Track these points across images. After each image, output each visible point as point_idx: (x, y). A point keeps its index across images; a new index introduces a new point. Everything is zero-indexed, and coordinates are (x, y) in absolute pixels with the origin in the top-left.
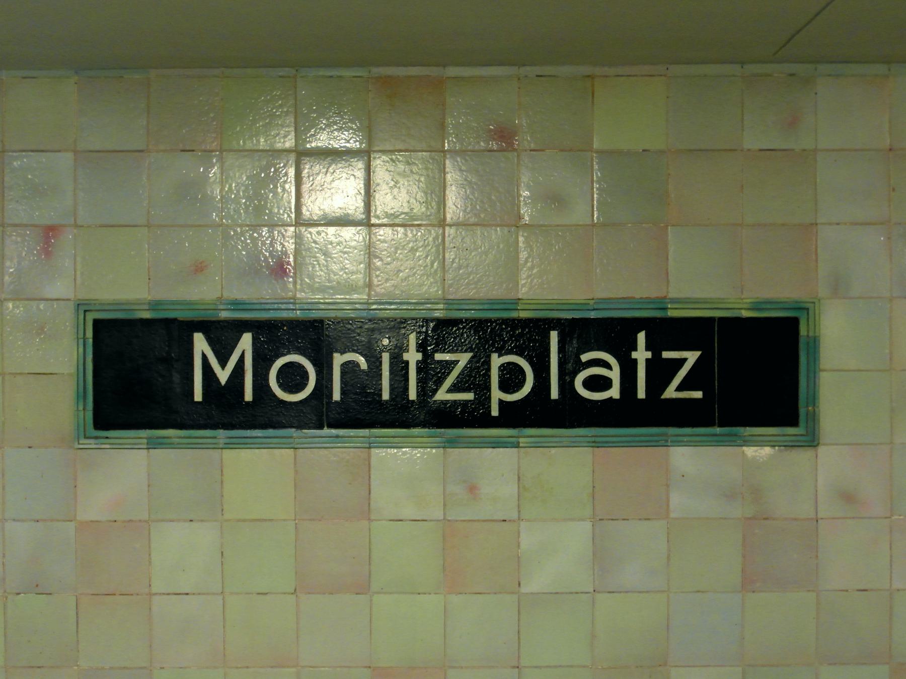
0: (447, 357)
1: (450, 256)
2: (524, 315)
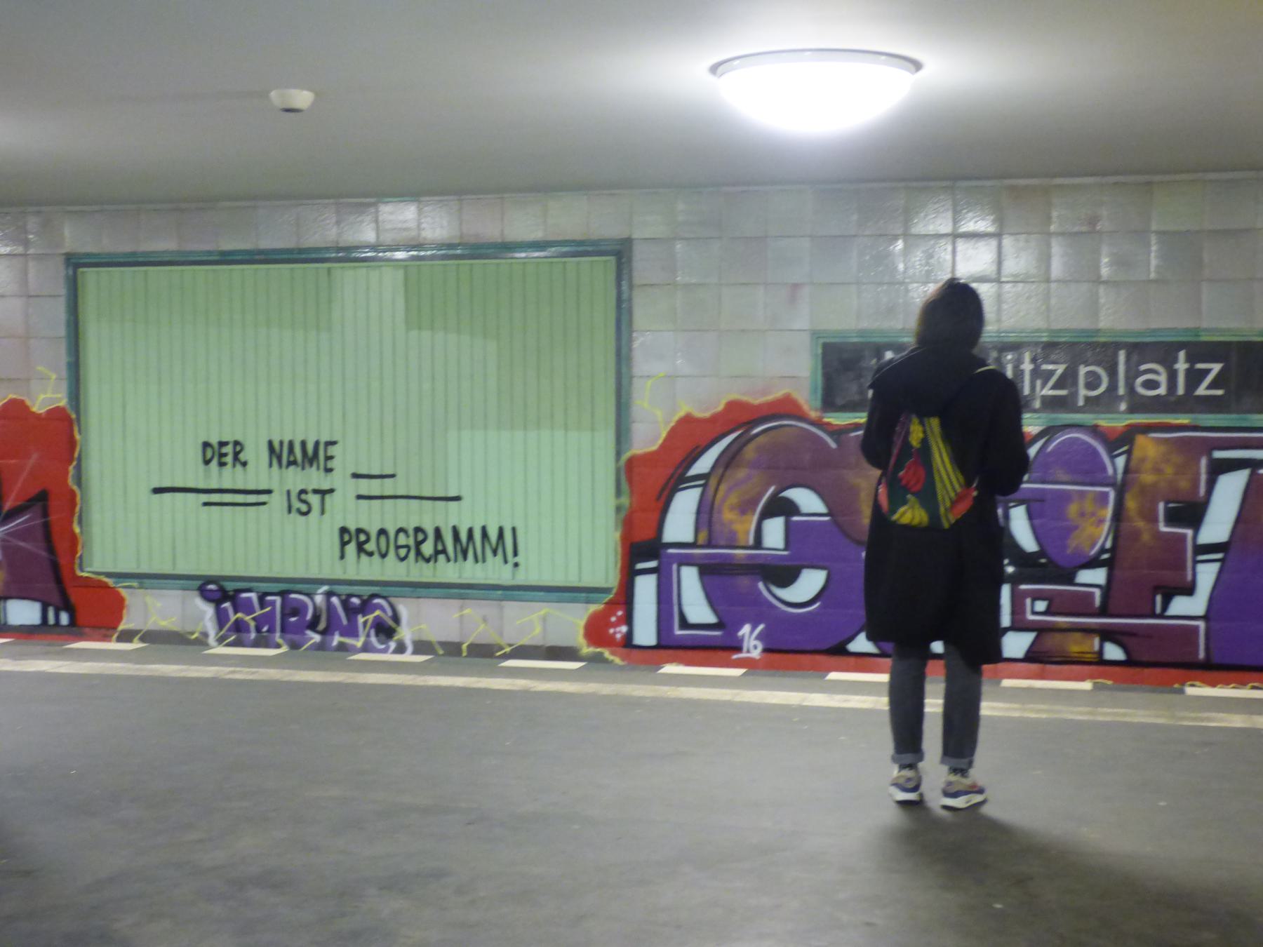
0: (1051, 367)
1: (1053, 301)
2: (1103, 340)
